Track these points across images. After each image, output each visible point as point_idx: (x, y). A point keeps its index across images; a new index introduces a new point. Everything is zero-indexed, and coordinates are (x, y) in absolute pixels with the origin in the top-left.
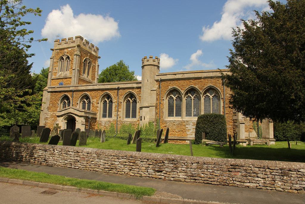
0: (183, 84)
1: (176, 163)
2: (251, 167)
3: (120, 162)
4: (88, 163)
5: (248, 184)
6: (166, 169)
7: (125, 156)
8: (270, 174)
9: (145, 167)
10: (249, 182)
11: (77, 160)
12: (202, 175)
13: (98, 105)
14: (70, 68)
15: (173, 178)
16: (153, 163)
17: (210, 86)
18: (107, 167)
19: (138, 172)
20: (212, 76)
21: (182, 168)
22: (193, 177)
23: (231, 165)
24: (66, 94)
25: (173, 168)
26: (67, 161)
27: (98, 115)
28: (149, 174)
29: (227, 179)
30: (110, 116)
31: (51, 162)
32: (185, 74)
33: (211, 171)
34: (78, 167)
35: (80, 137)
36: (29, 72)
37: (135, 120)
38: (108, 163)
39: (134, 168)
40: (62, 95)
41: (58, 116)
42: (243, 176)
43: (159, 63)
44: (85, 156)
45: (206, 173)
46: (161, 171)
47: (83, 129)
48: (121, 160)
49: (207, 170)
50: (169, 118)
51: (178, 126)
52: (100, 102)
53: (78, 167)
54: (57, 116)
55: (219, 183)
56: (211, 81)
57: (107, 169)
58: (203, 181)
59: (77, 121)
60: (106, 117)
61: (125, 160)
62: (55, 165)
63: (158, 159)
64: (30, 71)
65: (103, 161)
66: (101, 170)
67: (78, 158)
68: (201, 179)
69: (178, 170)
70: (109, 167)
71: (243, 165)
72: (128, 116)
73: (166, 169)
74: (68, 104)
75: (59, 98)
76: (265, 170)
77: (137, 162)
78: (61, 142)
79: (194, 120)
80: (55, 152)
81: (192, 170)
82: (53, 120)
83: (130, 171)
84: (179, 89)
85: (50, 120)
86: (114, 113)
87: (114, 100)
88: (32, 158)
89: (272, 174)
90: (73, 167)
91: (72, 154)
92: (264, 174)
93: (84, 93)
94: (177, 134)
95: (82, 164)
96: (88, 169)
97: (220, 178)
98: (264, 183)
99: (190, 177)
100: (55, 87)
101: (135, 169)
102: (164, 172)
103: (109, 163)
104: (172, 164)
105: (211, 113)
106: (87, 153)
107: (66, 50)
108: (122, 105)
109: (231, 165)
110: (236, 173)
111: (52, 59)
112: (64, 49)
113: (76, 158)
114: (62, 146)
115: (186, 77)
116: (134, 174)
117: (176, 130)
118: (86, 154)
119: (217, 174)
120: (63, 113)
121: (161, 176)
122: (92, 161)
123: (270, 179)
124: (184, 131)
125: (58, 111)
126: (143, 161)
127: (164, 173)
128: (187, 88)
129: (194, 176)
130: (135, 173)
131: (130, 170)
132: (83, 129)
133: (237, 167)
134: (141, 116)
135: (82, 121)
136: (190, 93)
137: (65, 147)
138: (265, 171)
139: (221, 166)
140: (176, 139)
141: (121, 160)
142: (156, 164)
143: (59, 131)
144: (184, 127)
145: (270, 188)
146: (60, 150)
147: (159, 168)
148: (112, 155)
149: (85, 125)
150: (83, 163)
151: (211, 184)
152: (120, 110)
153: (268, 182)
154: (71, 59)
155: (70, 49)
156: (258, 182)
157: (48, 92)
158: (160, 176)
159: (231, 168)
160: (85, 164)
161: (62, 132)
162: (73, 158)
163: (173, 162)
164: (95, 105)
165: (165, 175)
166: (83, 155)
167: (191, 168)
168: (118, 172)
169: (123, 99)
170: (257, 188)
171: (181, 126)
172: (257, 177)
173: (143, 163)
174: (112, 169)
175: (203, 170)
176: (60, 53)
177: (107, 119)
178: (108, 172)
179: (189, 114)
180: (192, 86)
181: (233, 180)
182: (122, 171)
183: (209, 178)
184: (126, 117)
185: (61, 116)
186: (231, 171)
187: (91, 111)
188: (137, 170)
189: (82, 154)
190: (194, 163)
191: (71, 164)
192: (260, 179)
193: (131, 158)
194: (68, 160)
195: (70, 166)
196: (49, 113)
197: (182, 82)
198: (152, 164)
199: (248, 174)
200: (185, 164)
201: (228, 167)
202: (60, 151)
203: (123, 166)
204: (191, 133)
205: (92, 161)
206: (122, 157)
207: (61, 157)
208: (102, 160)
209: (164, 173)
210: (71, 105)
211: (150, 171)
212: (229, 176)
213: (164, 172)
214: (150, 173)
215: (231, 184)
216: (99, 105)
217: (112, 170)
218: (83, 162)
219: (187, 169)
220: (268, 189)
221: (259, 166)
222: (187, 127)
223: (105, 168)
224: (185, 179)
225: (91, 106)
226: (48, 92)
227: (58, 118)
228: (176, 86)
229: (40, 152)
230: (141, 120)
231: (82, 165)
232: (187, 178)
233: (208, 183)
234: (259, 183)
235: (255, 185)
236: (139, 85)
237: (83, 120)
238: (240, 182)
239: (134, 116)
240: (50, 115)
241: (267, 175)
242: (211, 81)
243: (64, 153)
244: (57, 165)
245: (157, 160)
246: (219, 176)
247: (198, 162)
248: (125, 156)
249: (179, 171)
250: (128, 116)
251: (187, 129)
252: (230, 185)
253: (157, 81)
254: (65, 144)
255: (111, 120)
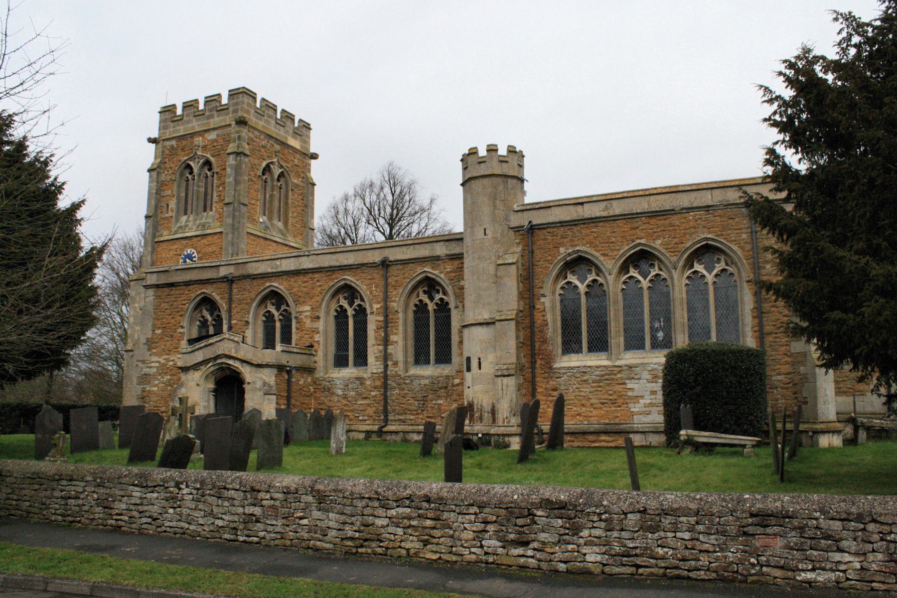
0: (608, 237)
1: (572, 513)
2: (816, 519)
3: (390, 518)
4: (288, 526)
5: (810, 576)
6: (543, 536)
7: (407, 498)
8: (882, 539)
9: (474, 532)
10: (813, 570)
11: (254, 515)
12: (660, 551)
13: (315, 325)
14: (215, 198)
15: (565, 562)
16: (498, 517)
17: (706, 239)
18: (350, 534)
19: (452, 547)
20: (710, 203)
21: (593, 531)
22: (631, 559)
23: (752, 515)
24: (208, 290)
25: (562, 531)
26: (222, 518)
27: (320, 357)
28: (486, 553)
29: (739, 559)
30: (361, 359)
31: (171, 524)
32: (615, 203)
33: (687, 536)
34: (256, 539)
35: (257, 441)
36: (21, 146)
37: (445, 370)
38: (352, 524)
39: (439, 535)
40: (193, 295)
41: (185, 369)
42: (792, 549)
43: (521, 166)
44: (278, 503)
45: (671, 542)
46: (525, 544)
47: (269, 410)
48: (393, 512)
49: (675, 532)
50: (566, 358)
51: (600, 386)
52: (322, 314)
53: (256, 539)
54: (180, 368)
55: (714, 575)
56: (706, 220)
57: (349, 543)
58: (662, 571)
59: (249, 383)
60: (346, 365)
61: (408, 510)
62: (184, 533)
63: (512, 505)
64: (63, 203)
65: (338, 516)
66: (332, 546)
67: (257, 511)
68: (656, 565)
69: (581, 537)
70: (357, 535)
71: (790, 514)
72: (421, 357)
73: (543, 536)
74: (214, 325)
75: (185, 304)
76: (862, 526)
77: (445, 515)
78: (197, 456)
79: (655, 360)
80: (185, 492)
81: (625, 534)
82: (169, 384)
83: (425, 545)
84: (597, 254)
85: (156, 382)
86: (373, 350)
87: (374, 308)
88: (111, 514)
89: (889, 538)
90: (241, 539)
91: (236, 496)
92: (859, 539)
93: (268, 284)
94: (595, 412)
95: (270, 528)
96: (288, 543)
97: (717, 559)
98: (862, 568)
99: (617, 558)
100: (167, 269)
101: (439, 538)
102: (535, 545)
103: (358, 523)
104: (561, 518)
105: (714, 339)
106: (284, 493)
107: (198, 140)
108: (401, 322)
109: (752, 515)
110: (769, 541)
111: (154, 174)
112: (193, 135)
113: (250, 510)
114: (205, 473)
115: (618, 212)
116: (438, 555)
117: (592, 401)
118: (280, 496)
119: (706, 547)
120: (199, 357)
121: (525, 559)
122: (301, 518)
123: (880, 556)
124: (621, 400)
125: (184, 351)
126: (465, 511)
127: (535, 549)
128: (622, 251)
129: (633, 556)
130: (441, 553)
131: (426, 543)
132: (269, 410)
133: (773, 521)
134: (466, 355)
135: (265, 384)
136: (636, 267)
137: (215, 474)
138: (864, 529)
139: (720, 517)
140: (592, 430)
141: (393, 512)
142: (508, 520)
143: (189, 421)
144: (618, 388)
145: (884, 587)
146: (198, 486)
147: (520, 533)
148: (363, 498)
149: (274, 397)
150: (273, 525)
151: (689, 578)
152: (393, 338)
153: (874, 567)
154: (216, 169)
155: (212, 136)
156: (843, 567)
157: (147, 287)
158: (522, 560)
159: (752, 525)
160: (279, 529)
161: (203, 422)
162: (241, 510)
163: (563, 511)
164: (308, 323)
165: (538, 555)
166: (272, 499)
167: (622, 530)
168: (387, 548)
169: (403, 298)
170: (841, 585)
171: (609, 385)
172: (840, 550)
173: (467, 517)
174: (366, 540)
175: (662, 534)
176: (179, 152)
177: (349, 372)
178: (354, 550)
179: (634, 342)
180: (643, 241)
181: (758, 563)
182: (400, 547)
183: (680, 560)
184: (417, 362)
185: (196, 367)
186: (753, 535)
187: (293, 344)
188: (449, 542)
189: (268, 496)
190: (631, 512)
191: (235, 528)
192: (847, 557)
193: (425, 505)
194: (224, 516)
195: (233, 537)
196: (155, 359)
197: (605, 230)
198: (495, 522)
199: (809, 541)
200: (603, 517)
201: (745, 521)
202: (198, 489)
203: (402, 530)
204: (647, 409)
205: (301, 518)
206: (396, 501)
207: (201, 506)
208: (332, 512)
209: (535, 549)
210: (225, 327)
211: (492, 543)
212: (746, 552)
213: (535, 545)
214: (490, 550)
215: (755, 578)
216: (320, 325)
217: (366, 543)
218: (274, 522)
219: (609, 533)
220: (877, 590)
221: (844, 516)
222: (629, 386)
223: (342, 539)
224: (604, 565)
225: (294, 330)
226: (147, 287)
227: (183, 377)
228: (584, 245)
229: (134, 494)
230: (469, 370)
231: (270, 532)
232: (610, 562)
233: (678, 577)
234: (844, 571)
235: (832, 576)
236: (455, 249)
237: (269, 377)
238: (782, 568)
239: (444, 357)
240: (157, 364)
241: (872, 543)
242: (706, 220)
243: (210, 495)
244: (192, 534)
245: (512, 508)
246: (715, 552)
247: (645, 510)
248: (407, 498)
249: (582, 541)
250: (421, 357)
251: (630, 393)
252: (750, 579)
253: (517, 229)
254: (210, 465)
255: (366, 376)
